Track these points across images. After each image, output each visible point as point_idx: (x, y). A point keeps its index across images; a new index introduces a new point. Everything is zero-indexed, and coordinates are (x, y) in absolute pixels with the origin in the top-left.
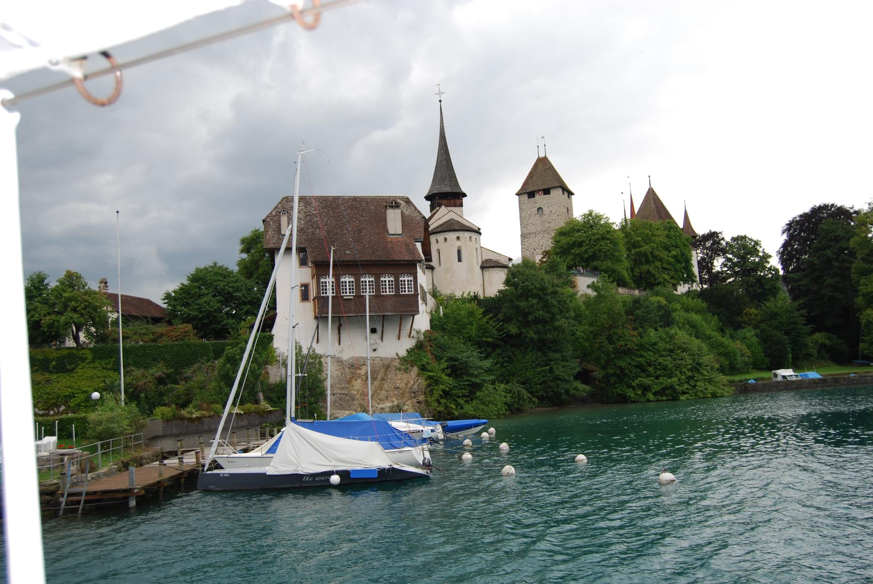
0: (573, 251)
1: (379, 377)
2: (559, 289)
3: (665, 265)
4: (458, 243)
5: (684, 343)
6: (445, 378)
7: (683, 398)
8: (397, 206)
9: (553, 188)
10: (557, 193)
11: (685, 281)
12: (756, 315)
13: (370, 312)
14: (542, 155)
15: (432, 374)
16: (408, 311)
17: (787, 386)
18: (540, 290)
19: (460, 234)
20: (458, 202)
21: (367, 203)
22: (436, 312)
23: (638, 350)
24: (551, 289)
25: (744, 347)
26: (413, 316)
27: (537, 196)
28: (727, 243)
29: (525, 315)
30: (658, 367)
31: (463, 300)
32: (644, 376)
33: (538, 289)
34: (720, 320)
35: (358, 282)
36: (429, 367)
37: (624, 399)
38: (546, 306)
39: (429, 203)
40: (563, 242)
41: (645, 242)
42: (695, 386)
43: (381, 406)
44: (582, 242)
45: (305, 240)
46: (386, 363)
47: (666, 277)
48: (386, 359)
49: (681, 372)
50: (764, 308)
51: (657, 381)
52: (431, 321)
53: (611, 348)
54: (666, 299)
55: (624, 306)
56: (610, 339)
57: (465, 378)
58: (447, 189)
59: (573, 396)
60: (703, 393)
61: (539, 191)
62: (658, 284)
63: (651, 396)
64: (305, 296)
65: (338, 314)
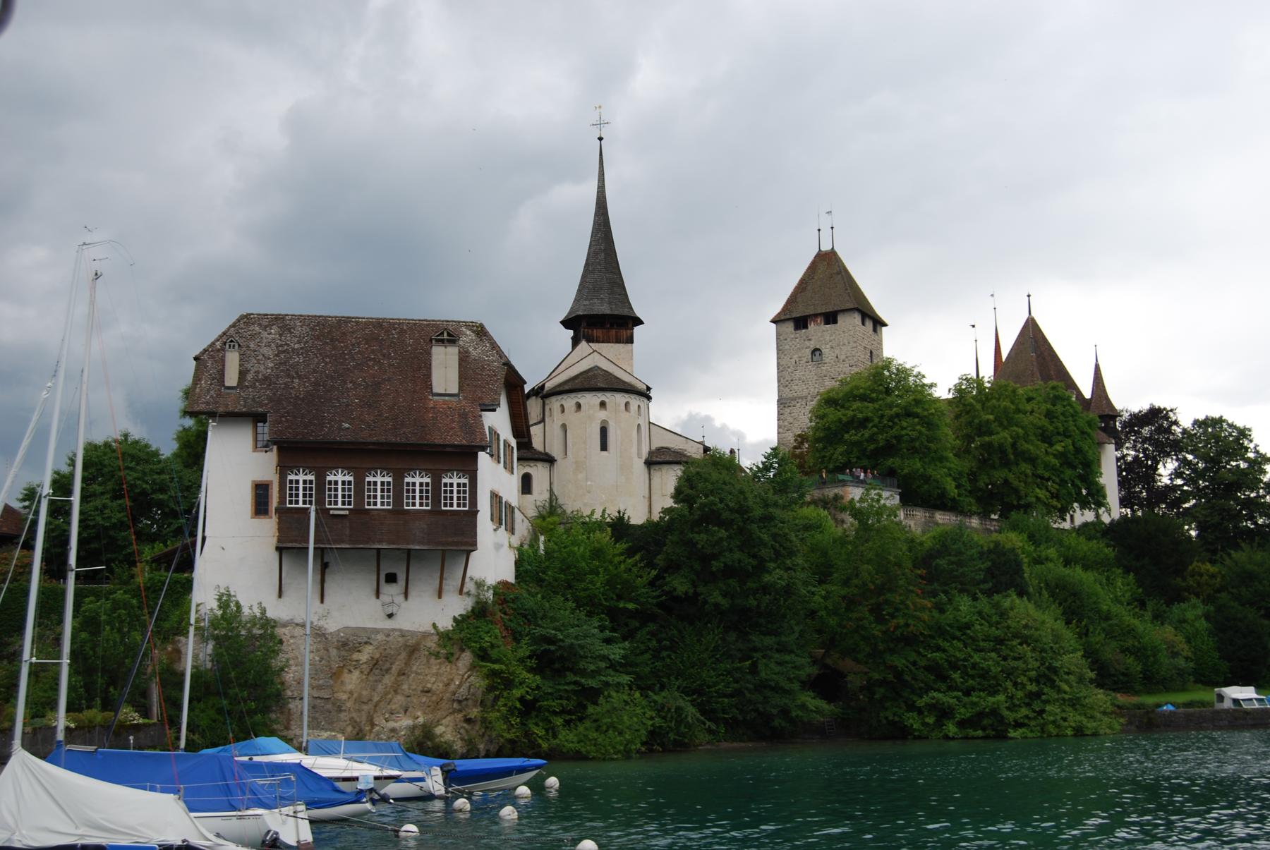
0: (846, 436)
1: (395, 669)
2: (777, 512)
3: (1040, 471)
4: (603, 415)
5: (1026, 626)
6: (525, 674)
7: (1012, 734)
10: (850, 322)
11: (1084, 505)
12: (1213, 576)
13: (316, 542)
14: (826, 247)
15: (497, 667)
16: (457, 544)
17: (1240, 718)
18: (737, 512)
19: (608, 397)
20: (624, 333)
22: (531, 546)
23: (932, 637)
24: (758, 512)
25: (1180, 638)
26: (468, 553)
27: (812, 327)
28: (1184, 431)
29: (706, 559)
30: (971, 672)
31: (591, 527)
32: (944, 687)
33: (732, 510)
34: (1140, 583)
35: (359, 482)
36: (494, 653)
37: (901, 733)
39: (571, 333)
40: (831, 417)
41: (1001, 425)
42: (1042, 712)
43: (391, 724)
44: (867, 420)
45: (270, 399)
46: (412, 642)
47: (1042, 494)
48: (413, 633)
49: (1015, 684)
50: (1228, 562)
51: (966, 699)
52: (518, 564)
53: (877, 630)
54: (1031, 537)
55: (910, 550)
56: (876, 610)
57: (571, 677)
58: (604, 309)
60: (1058, 727)
61: (816, 315)
62: (1018, 507)
63: (951, 728)
64: (261, 507)
65: (316, 542)
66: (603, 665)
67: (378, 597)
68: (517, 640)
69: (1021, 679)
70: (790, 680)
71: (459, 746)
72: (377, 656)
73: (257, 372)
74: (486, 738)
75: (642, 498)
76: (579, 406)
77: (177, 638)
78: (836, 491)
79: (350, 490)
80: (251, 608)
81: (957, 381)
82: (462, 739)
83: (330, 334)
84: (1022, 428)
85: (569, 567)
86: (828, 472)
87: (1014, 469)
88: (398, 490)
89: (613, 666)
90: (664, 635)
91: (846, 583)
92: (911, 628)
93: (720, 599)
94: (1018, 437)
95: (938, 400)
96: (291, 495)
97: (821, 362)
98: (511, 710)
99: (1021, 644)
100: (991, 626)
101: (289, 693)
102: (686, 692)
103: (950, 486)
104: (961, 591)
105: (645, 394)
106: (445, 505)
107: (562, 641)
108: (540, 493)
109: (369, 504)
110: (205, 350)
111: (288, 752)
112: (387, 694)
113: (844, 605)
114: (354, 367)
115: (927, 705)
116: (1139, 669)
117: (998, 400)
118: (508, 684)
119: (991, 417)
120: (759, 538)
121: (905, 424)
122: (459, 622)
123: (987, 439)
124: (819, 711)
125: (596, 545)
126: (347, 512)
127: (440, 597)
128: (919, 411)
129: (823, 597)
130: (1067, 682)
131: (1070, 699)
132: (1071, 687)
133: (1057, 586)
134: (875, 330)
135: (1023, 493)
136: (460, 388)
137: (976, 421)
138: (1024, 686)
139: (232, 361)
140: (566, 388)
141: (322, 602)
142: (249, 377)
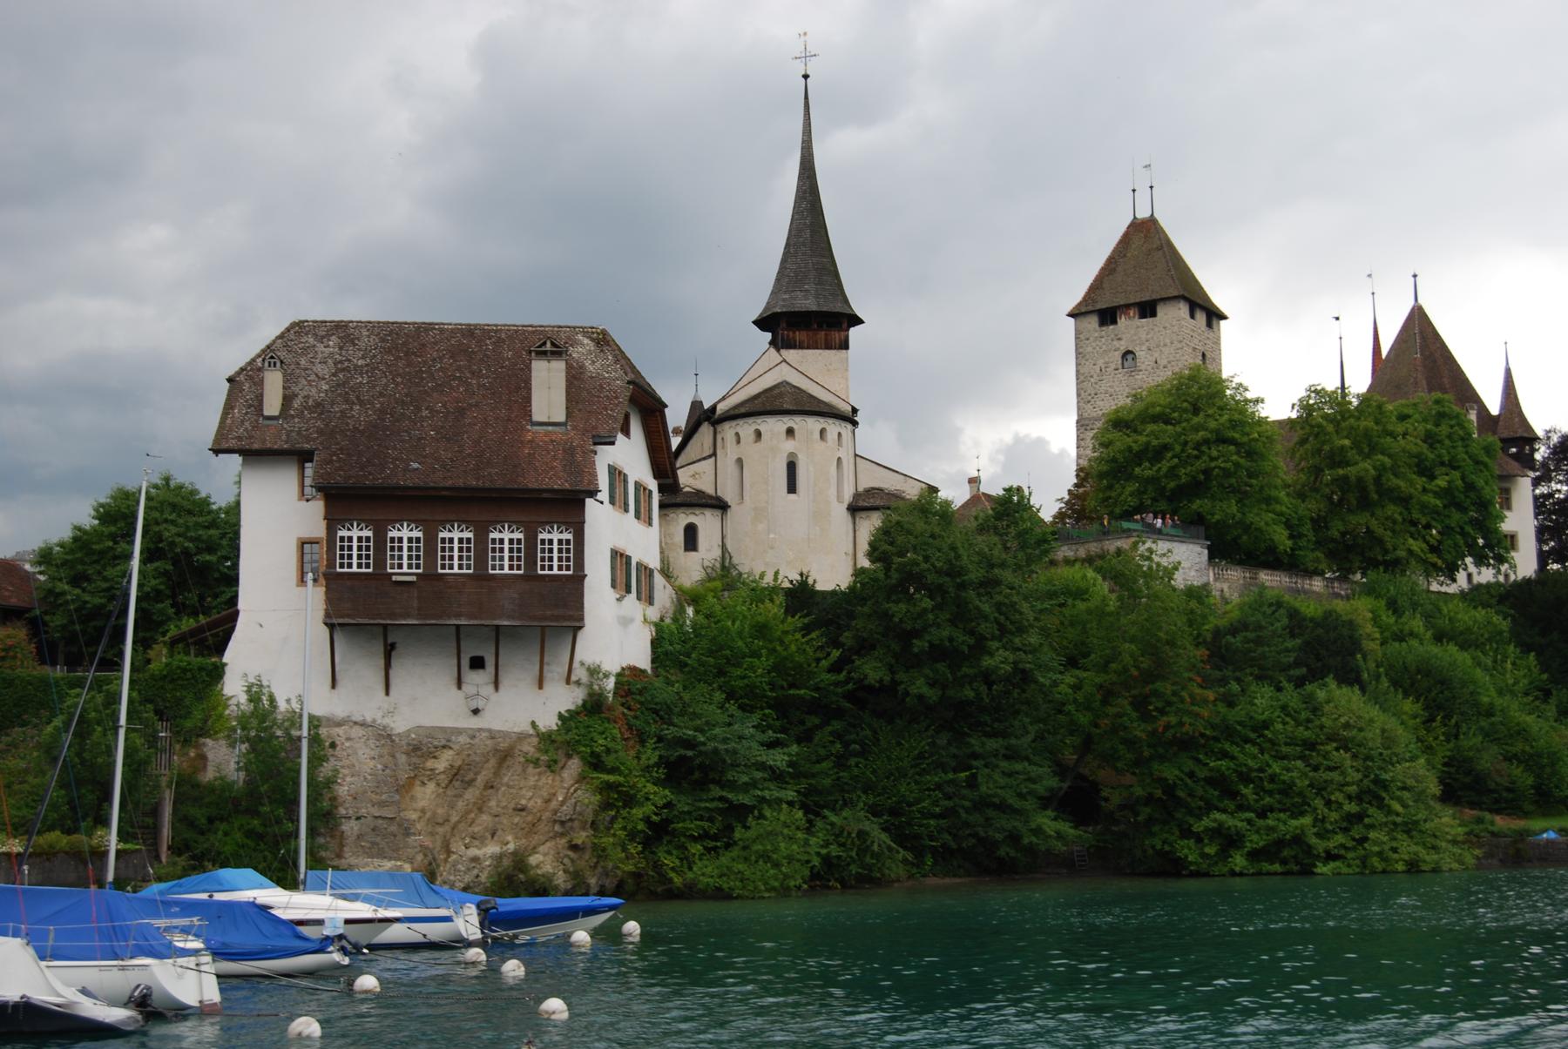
1: (480, 780)
2: (1007, 575)
4: (789, 446)
5: (1347, 726)
6: (651, 788)
7: (1322, 869)
8: (557, 352)
9: (1165, 300)
10: (1174, 315)
11: (1480, 561)
14: (1143, 214)
15: (612, 778)
16: (557, 618)
18: (948, 574)
19: (796, 422)
20: (836, 336)
21: (499, 342)
22: (675, 620)
23: (1216, 739)
24: (975, 574)
27: (1122, 321)
29: (907, 636)
31: (761, 594)
32: (1232, 806)
33: (939, 572)
34: (1545, 668)
35: (431, 539)
36: (610, 761)
37: (1172, 867)
38: (962, 615)
41: (1360, 452)
42: (1365, 839)
44: (1166, 447)
45: (320, 432)
46: (503, 745)
47: (1416, 545)
48: (505, 734)
49: (1328, 803)
51: (1260, 823)
52: (655, 643)
53: (1140, 731)
56: (1140, 704)
57: (716, 791)
58: (808, 303)
59: (1031, 850)
60: (1385, 859)
61: (1128, 306)
65: (367, 614)
66: (758, 775)
67: (459, 687)
68: (642, 742)
69: (1337, 796)
70: (1021, 796)
71: (561, 880)
72: (458, 763)
73: (308, 397)
74: (600, 870)
75: (831, 557)
76: (758, 434)
77: (202, 740)
78: (1119, 543)
79: (418, 549)
80: (288, 701)
81: (1304, 394)
82: (565, 871)
83: (404, 343)
84: (1390, 456)
85: (721, 648)
86: (1112, 516)
87: (1379, 512)
88: (481, 549)
89: (777, 776)
90: (853, 737)
91: (1104, 667)
92: (1187, 728)
93: (926, 690)
94: (1385, 469)
95: (1263, 422)
96: (342, 557)
97: (1135, 369)
98: (632, 835)
99: (1337, 749)
100: (1298, 724)
101: (342, 811)
102: (874, 811)
103: (1281, 538)
104: (1259, 678)
105: (850, 418)
106: (543, 568)
107: (704, 744)
108: (709, 549)
109: (443, 567)
110: (242, 369)
111: (261, 887)
112: (468, 812)
113: (1099, 697)
114: (432, 389)
115: (1207, 830)
116: (1530, 781)
117: (1358, 419)
118: (629, 800)
119: (1347, 442)
120: (977, 608)
121: (1215, 453)
122: (566, 719)
123: (1341, 472)
124: (1060, 836)
125: (760, 619)
126: (414, 578)
127: (541, 687)
128: (1237, 436)
129: (1070, 686)
130: (1400, 800)
131: (1405, 824)
132: (1405, 806)
133: (1419, 671)
134: (1209, 325)
135: (1389, 546)
136: (569, 415)
137: (1327, 447)
138: (1340, 805)
139: (274, 385)
140: (743, 410)
141: (387, 693)
142: (296, 403)
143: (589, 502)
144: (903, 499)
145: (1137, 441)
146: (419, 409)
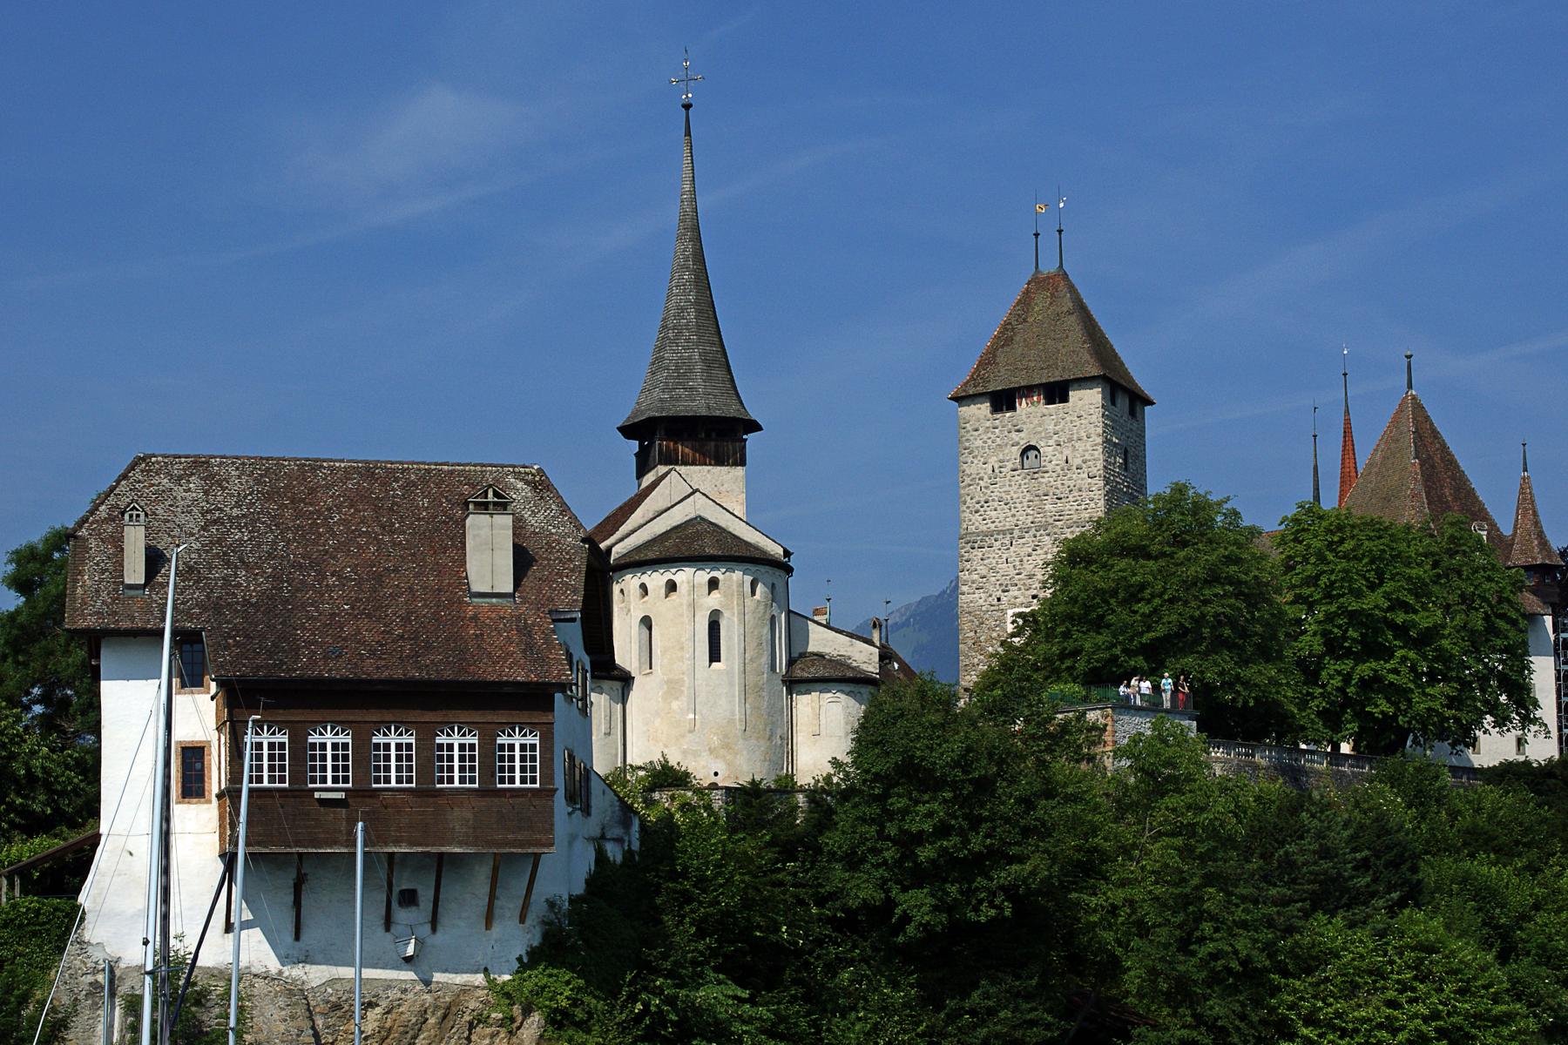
4: (715, 600)
14: (1049, 267)
27: (1023, 406)
35: (363, 747)
39: (634, 445)
44: (1142, 587)
67: (388, 929)
97: (1039, 471)
126: (341, 795)
127: (488, 926)
134: (1132, 413)
140: (651, 555)
141: (297, 938)
143: (558, 696)
144: (849, 667)
145: (1097, 579)
146: (321, 576)
